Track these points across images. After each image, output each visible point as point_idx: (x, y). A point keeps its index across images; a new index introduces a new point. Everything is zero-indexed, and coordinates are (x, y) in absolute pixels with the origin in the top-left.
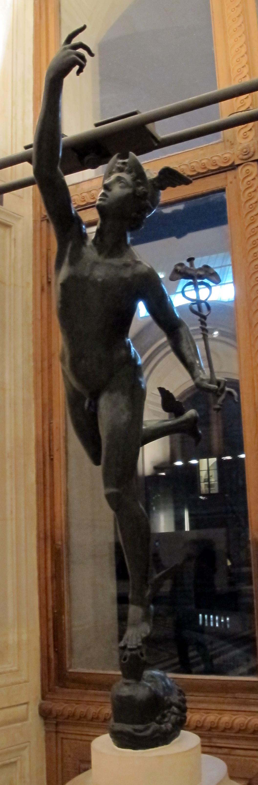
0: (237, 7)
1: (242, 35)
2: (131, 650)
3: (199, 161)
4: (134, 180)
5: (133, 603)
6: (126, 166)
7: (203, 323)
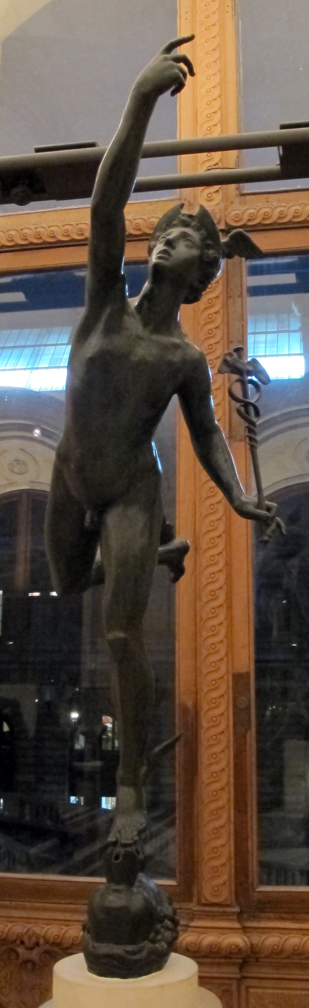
0: (213, 37)
1: (216, 73)
2: (125, 846)
3: (146, 219)
4: (203, 240)
5: (123, 783)
6: (194, 220)
7: (251, 431)
